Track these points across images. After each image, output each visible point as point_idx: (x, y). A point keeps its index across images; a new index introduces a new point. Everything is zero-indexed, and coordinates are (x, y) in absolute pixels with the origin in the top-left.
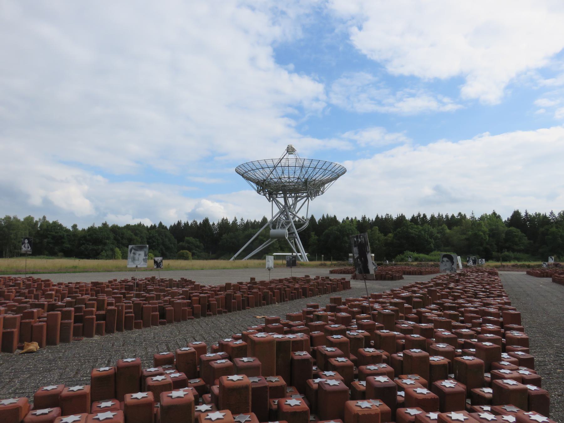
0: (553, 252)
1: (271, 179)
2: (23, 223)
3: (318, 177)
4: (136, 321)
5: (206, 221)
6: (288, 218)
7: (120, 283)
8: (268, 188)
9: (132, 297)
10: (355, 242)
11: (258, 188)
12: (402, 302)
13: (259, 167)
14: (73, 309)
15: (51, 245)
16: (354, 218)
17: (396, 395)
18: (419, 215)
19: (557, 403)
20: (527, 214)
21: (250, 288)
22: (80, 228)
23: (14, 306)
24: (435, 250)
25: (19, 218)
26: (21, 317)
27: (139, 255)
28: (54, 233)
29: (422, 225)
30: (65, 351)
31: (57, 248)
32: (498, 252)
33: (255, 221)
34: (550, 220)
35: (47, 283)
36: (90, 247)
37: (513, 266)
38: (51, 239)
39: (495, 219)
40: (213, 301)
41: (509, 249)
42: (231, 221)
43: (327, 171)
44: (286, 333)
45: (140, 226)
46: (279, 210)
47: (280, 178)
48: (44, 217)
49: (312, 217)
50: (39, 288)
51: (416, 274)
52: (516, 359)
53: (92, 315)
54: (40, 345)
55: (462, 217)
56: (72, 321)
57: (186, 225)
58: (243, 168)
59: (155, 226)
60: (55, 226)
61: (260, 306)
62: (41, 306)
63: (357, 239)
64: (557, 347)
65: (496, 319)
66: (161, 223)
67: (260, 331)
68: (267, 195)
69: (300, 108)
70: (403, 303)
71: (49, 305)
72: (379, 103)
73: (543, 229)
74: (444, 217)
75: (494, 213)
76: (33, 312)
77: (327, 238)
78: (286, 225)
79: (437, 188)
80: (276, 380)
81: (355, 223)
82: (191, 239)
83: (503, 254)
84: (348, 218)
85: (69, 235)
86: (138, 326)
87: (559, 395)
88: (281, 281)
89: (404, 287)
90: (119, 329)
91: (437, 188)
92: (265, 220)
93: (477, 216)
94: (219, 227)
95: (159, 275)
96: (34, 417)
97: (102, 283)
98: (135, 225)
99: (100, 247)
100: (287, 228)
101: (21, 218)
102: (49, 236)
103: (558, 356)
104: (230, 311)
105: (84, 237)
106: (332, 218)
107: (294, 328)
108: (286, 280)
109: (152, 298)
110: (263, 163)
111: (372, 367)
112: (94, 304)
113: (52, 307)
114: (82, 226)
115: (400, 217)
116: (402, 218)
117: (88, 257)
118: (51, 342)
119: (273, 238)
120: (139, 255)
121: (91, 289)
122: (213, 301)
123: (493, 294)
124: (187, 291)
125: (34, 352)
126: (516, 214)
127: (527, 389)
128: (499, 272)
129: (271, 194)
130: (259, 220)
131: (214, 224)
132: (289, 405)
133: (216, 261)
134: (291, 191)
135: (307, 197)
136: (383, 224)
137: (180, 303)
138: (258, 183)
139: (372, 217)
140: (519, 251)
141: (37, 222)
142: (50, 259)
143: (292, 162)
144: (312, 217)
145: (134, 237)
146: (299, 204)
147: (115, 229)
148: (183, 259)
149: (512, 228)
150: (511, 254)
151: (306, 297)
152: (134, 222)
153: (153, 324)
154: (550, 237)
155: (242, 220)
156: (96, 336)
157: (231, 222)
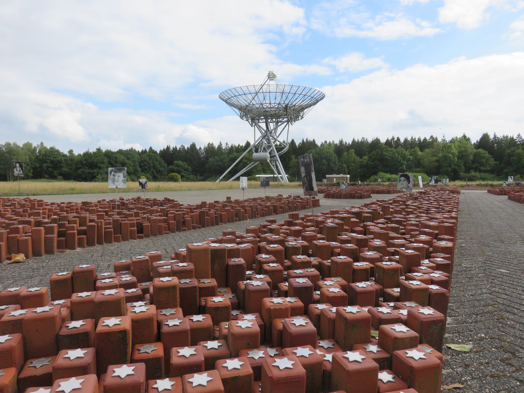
0: (515, 173)
1: (253, 105)
2: (22, 149)
3: (298, 102)
4: (115, 235)
5: (193, 146)
6: (269, 142)
7: (108, 202)
8: (251, 114)
9: (114, 215)
10: (302, 161)
11: (241, 114)
12: (349, 217)
13: (241, 93)
14: (55, 225)
15: (50, 169)
16: (331, 142)
17: (312, 294)
18: (393, 139)
19: (468, 301)
20: (495, 136)
21: (224, 206)
22: (76, 153)
23: (4, 223)
24: (406, 171)
25: (18, 144)
26: (8, 232)
27: (119, 176)
28: (52, 158)
29: (396, 147)
30: (49, 261)
31: (56, 173)
32: (466, 172)
33: (239, 145)
34: (516, 142)
35: (41, 203)
36: (87, 171)
37: (478, 185)
38: (48, 165)
39: (465, 141)
40: (188, 218)
41: (476, 169)
42: (216, 145)
43: (306, 97)
44: (238, 243)
45: (132, 150)
46: (261, 135)
47: (262, 104)
48: (42, 143)
49: (293, 141)
50: (33, 207)
51: (384, 193)
52: (434, 265)
53: (74, 230)
54: (27, 257)
55: (434, 140)
56: (55, 235)
57: (175, 149)
58: (226, 94)
59: (146, 150)
60: (52, 152)
61: (233, 222)
62: (29, 223)
63: (304, 159)
64: (488, 255)
65: (431, 231)
66: (151, 148)
67: (213, 242)
68: (250, 120)
69: (280, 33)
70: (350, 218)
71: (36, 222)
72: (359, 28)
73: (509, 151)
74: (417, 140)
75: (464, 136)
76: (18, 227)
77: (302, 159)
78: (268, 149)
79: (411, 113)
80: (209, 282)
81: (332, 146)
82: (180, 163)
83: (470, 174)
84: (326, 142)
85: (67, 160)
86: (117, 240)
87: (471, 295)
88: (255, 200)
89: (365, 204)
90: (100, 243)
91: (411, 113)
92: (248, 144)
93: (448, 139)
94: (205, 152)
95: (144, 196)
96: (34, 314)
97: (91, 203)
98: (127, 151)
99: (96, 171)
100: (268, 152)
101: (21, 144)
102: (48, 161)
103: (485, 263)
104: (204, 226)
105: (81, 161)
106: (311, 142)
107: (244, 240)
108: (261, 199)
109: (131, 215)
110: (245, 89)
111: (298, 271)
112: (76, 221)
113: (38, 224)
114: (78, 151)
115: (375, 140)
116: (376, 142)
117: (85, 180)
118: (37, 253)
119: (256, 161)
120: (119, 176)
121: (81, 209)
122: (189, 217)
123: (444, 209)
124: (165, 209)
125: (21, 262)
126: (485, 137)
127: (428, 289)
128: (462, 191)
129: (253, 120)
130: (243, 144)
131: (200, 148)
132: (214, 301)
133: (203, 182)
134: (272, 116)
135: (288, 122)
136: (359, 147)
137: (156, 220)
138: (240, 109)
139: (348, 141)
140: (485, 171)
141: (35, 148)
142: (50, 182)
143: (273, 89)
144: (293, 141)
145: (127, 161)
146: (280, 129)
147: (109, 154)
148: (173, 181)
149: (481, 150)
150: (478, 174)
151: (277, 214)
152: (126, 147)
153: (131, 238)
154: (515, 158)
155: (227, 144)
156: (78, 248)
157: (216, 147)
